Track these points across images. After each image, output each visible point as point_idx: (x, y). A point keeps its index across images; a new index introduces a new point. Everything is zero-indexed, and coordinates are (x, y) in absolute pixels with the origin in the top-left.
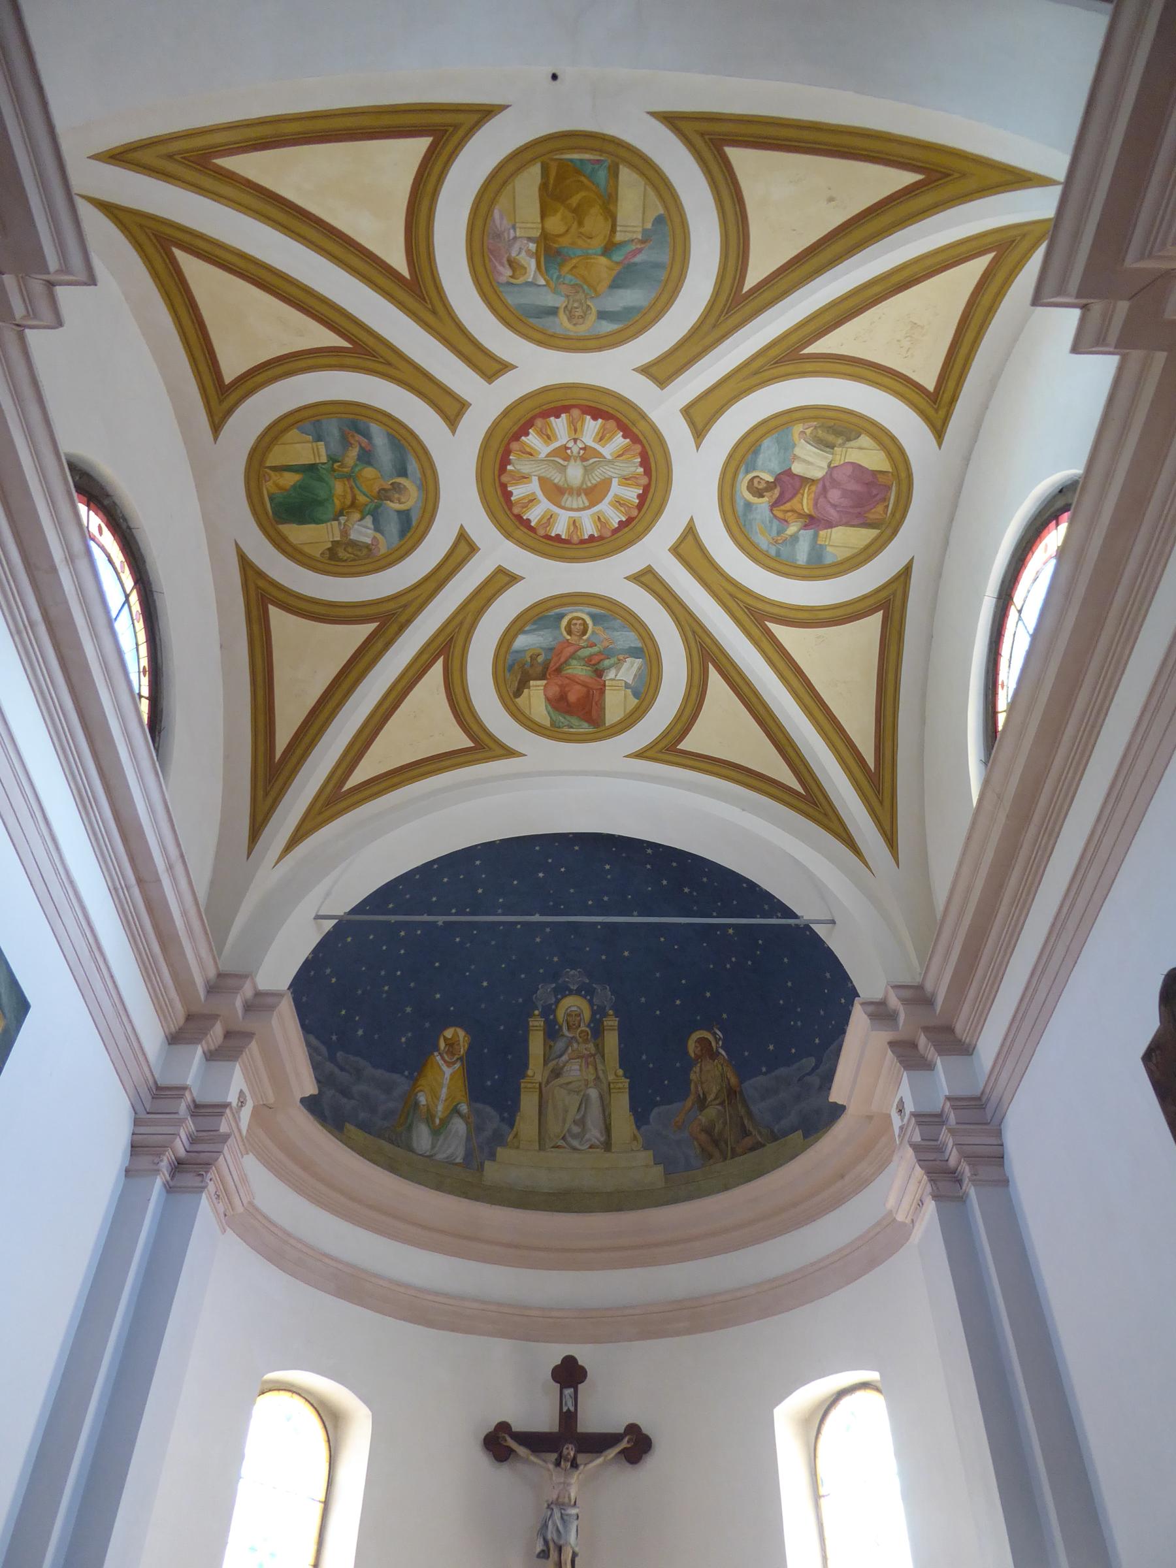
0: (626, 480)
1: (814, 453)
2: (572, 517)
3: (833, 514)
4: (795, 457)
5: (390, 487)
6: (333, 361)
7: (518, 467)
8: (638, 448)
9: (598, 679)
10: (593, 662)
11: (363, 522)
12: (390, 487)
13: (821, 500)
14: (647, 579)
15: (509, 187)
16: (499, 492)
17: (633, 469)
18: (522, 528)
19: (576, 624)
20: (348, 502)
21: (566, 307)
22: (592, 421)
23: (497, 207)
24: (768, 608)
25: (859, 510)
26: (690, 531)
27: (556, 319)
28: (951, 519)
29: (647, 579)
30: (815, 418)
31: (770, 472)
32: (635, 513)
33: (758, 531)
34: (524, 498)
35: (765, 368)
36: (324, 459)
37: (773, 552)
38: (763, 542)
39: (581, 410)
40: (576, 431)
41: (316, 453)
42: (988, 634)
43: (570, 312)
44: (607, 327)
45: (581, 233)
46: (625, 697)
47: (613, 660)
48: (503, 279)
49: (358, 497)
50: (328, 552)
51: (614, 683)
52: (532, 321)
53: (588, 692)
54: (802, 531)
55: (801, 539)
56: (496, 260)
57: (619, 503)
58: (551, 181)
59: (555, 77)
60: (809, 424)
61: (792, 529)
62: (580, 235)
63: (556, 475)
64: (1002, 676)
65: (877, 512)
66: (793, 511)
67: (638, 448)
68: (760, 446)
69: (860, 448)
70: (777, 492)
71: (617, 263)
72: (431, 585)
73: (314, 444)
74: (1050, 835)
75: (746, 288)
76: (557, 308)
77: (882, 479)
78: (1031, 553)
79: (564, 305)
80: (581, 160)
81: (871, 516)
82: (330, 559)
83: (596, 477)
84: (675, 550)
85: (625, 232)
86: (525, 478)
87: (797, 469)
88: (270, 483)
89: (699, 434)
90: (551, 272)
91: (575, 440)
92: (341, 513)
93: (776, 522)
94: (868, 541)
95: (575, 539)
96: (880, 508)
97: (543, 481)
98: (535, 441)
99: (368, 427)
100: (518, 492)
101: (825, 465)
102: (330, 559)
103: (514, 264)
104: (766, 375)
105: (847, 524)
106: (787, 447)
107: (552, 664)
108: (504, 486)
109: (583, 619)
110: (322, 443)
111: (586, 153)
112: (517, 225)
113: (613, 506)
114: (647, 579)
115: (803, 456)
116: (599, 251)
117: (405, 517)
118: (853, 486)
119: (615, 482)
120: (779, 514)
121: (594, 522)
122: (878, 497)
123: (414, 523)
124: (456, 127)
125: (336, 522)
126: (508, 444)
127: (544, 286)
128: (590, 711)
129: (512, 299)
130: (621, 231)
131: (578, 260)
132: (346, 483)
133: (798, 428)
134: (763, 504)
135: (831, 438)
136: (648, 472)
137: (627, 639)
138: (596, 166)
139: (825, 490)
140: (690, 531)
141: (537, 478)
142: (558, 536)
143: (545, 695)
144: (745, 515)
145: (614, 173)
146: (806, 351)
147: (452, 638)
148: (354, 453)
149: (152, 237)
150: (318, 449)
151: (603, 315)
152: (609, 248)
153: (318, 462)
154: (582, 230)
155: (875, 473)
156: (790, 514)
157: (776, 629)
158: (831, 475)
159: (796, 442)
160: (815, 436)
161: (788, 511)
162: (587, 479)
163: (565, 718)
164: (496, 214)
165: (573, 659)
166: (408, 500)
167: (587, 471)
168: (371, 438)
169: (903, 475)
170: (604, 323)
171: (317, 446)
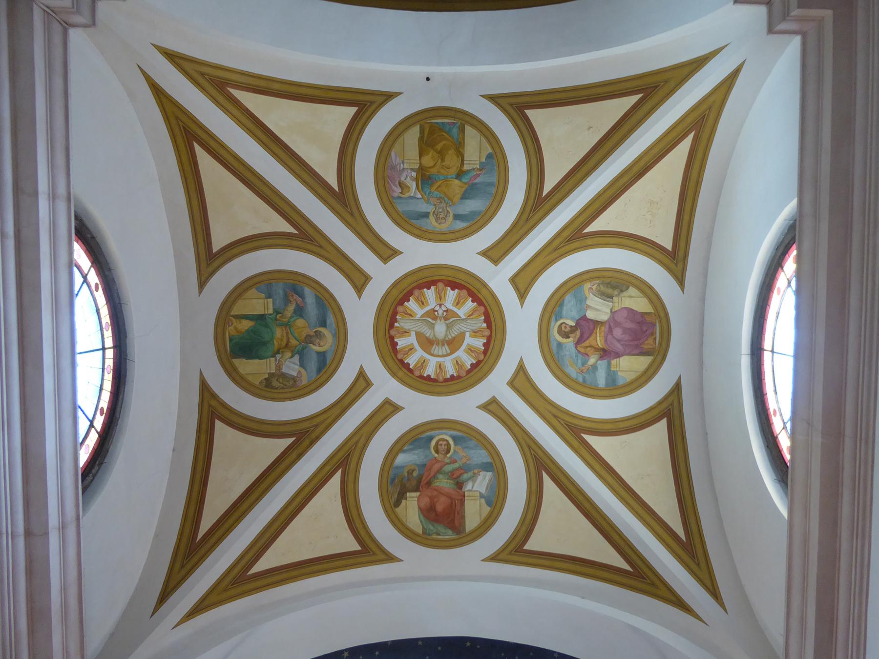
0: (475, 333)
1: (600, 303)
2: (438, 362)
3: (619, 347)
4: (588, 307)
5: (314, 334)
6: (285, 242)
7: (402, 324)
8: (482, 309)
9: (458, 490)
10: (455, 476)
11: (292, 360)
12: (313, 334)
13: (610, 337)
14: (493, 407)
15: (400, 140)
16: (388, 342)
17: (480, 325)
18: (403, 369)
19: (441, 445)
20: (284, 344)
21: (434, 212)
22: (451, 291)
23: (393, 150)
24: (583, 424)
25: (636, 343)
26: (521, 369)
27: (428, 220)
28: (701, 344)
29: (493, 407)
30: (598, 278)
31: (572, 319)
32: (482, 357)
33: (569, 365)
34: (405, 348)
35: (562, 245)
36: (271, 311)
37: (581, 380)
38: (572, 372)
39: (444, 283)
40: (441, 299)
41: (266, 307)
42: (751, 388)
43: (437, 215)
44: (460, 225)
45: (443, 165)
46: (480, 506)
47: (470, 474)
48: (396, 195)
49: (291, 340)
50: (265, 382)
51: (471, 494)
52: (414, 222)
53: (452, 503)
54: (599, 362)
55: (599, 367)
56: (392, 182)
57: (471, 350)
58: (426, 136)
59: (428, 79)
60: (594, 282)
61: (592, 360)
62: (443, 167)
63: (427, 331)
64: (772, 405)
65: (648, 344)
66: (591, 346)
67: (482, 309)
68: (563, 301)
69: (631, 297)
70: (578, 333)
71: (466, 183)
72: (336, 411)
73: (266, 300)
74: (867, 443)
75: (545, 193)
76: (429, 213)
77: (648, 319)
78: (768, 307)
79: (433, 211)
80: (443, 123)
81: (645, 347)
82: (266, 386)
83: (454, 332)
84: (511, 384)
85: (469, 164)
86: (406, 332)
87: (590, 315)
88: (232, 328)
89: (522, 295)
90: (425, 190)
91: (440, 305)
92: (278, 352)
93: (580, 356)
94: (646, 366)
95: (441, 379)
96: (650, 341)
97: (419, 335)
98: (414, 359)
99: (303, 290)
100: (402, 342)
101: (609, 311)
102: (266, 386)
103: (402, 185)
104: (562, 250)
105: (629, 354)
106: (581, 300)
107: (424, 478)
108: (392, 338)
109: (446, 440)
110: (271, 299)
111: (446, 119)
112: (405, 161)
113: (467, 353)
114: (492, 407)
115: (593, 306)
116: (454, 176)
117: (322, 356)
118: (629, 325)
119: (468, 335)
120: (582, 350)
121: (454, 365)
122: (647, 333)
123: (328, 362)
124: (372, 103)
125: (274, 358)
126: (396, 307)
127: (421, 198)
128: (453, 520)
129: (401, 207)
130: (467, 164)
131: (441, 182)
132: (284, 329)
133: (587, 286)
134: (569, 342)
135: (609, 291)
136: (489, 327)
137: (480, 456)
138: (452, 126)
139: (610, 330)
140: (521, 369)
141: (414, 332)
142: (429, 376)
143: (418, 506)
144: (558, 353)
145: (462, 130)
146: (586, 231)
147: (349, 454)
148: (291, 308)
149: (182, 128)
150: (267, 303)
151: (457, 217)
152: (460, 175)
153: (266, 313)
154: (444, 164)
155: (643, 314)
156: (589, 349)
157: (590, 439)
158: (613, 318)
159: (587, 297)
160: (599, 291)
161: (587, 347)
162: (448, 333)
163: (434, 526)
164: (393, 154)
165: (440, 473)
166: (324, 345)
167: (449, 327)
168: (304, 298)
169: (662, 315)
170: (458, 222)
171: (267, 301)
